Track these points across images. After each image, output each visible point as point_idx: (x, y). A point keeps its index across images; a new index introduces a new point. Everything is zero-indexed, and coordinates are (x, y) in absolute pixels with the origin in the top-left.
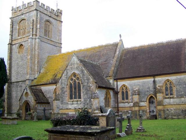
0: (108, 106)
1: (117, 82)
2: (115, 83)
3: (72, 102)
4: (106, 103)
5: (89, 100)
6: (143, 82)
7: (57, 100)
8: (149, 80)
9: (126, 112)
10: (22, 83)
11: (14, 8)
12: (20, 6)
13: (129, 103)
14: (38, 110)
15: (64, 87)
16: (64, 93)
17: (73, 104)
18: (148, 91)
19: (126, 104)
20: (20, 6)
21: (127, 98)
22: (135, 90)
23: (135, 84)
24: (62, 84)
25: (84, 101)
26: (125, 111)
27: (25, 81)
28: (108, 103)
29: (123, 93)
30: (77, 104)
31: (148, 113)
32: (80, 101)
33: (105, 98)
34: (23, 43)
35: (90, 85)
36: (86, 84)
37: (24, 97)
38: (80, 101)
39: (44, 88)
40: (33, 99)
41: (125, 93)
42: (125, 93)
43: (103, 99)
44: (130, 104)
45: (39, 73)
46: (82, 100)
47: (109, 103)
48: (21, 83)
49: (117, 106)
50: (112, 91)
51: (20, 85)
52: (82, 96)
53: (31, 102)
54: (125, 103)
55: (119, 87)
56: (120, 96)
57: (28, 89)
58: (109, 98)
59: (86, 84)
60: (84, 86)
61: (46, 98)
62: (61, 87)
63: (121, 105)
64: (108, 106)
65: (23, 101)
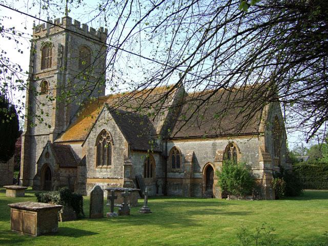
0: (150, 176)
1: (166, 143)
2: (164, 144)
3: (100, 169)
4: (147, 172)
5: (120, 167)
6: (200, 144)
7: (81, 166)
8: (191, 142)
9: (176, 184)
10: (44, 138)
11: (36, 26)
12: (59, 19)
13: (180, 173)
14: (61, 178)
15: (91, 149)
16: (91, 156)
17: (101, 171)
18: (205, 158)
19: (177, 173)
20: (59, 19)
21: (179, 167)
22: (188, 155)
23: (189, 146)
24: (89, 144)
25: (115, 168)
26: (175, 183)
27: (48, 135)
28: (150, 172)
29: (173, 157)
30: (107, 172)
31: (203, 188)
32: (110, 168)
33: (145, 164)
34: (226, 36)
35: (123, 147)
36: (118, 146)
37: (44, 158)
38: (110, 168)
39: (73, 146)
40: (55, 161)
41: (176, 158)
42: (176, 158)
43: (141, 167)
44: (181, 174)
45: (69, 124)
46: (112, 166)
47: (151, 172)
48: (43, 136)
49: (164, 177)
50: (158, 156)
51: (42, 140)
52: (112, 162)
53: (52, 166)
54: (175, 172)
55: (169, 150)
56: (169, 162)
57: (49, 147)
58: (151, 165)
59: (118, 146)
60: (115, 148)
61: (75, 160)
62: (88, 148)
63: (170, 175)
64: (150, 176)
65: (43, 164)
